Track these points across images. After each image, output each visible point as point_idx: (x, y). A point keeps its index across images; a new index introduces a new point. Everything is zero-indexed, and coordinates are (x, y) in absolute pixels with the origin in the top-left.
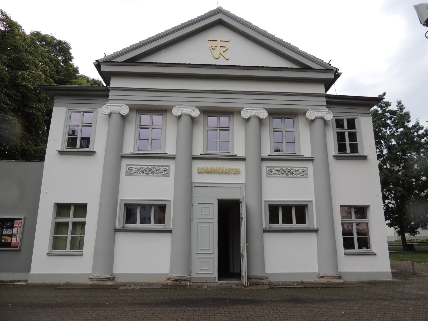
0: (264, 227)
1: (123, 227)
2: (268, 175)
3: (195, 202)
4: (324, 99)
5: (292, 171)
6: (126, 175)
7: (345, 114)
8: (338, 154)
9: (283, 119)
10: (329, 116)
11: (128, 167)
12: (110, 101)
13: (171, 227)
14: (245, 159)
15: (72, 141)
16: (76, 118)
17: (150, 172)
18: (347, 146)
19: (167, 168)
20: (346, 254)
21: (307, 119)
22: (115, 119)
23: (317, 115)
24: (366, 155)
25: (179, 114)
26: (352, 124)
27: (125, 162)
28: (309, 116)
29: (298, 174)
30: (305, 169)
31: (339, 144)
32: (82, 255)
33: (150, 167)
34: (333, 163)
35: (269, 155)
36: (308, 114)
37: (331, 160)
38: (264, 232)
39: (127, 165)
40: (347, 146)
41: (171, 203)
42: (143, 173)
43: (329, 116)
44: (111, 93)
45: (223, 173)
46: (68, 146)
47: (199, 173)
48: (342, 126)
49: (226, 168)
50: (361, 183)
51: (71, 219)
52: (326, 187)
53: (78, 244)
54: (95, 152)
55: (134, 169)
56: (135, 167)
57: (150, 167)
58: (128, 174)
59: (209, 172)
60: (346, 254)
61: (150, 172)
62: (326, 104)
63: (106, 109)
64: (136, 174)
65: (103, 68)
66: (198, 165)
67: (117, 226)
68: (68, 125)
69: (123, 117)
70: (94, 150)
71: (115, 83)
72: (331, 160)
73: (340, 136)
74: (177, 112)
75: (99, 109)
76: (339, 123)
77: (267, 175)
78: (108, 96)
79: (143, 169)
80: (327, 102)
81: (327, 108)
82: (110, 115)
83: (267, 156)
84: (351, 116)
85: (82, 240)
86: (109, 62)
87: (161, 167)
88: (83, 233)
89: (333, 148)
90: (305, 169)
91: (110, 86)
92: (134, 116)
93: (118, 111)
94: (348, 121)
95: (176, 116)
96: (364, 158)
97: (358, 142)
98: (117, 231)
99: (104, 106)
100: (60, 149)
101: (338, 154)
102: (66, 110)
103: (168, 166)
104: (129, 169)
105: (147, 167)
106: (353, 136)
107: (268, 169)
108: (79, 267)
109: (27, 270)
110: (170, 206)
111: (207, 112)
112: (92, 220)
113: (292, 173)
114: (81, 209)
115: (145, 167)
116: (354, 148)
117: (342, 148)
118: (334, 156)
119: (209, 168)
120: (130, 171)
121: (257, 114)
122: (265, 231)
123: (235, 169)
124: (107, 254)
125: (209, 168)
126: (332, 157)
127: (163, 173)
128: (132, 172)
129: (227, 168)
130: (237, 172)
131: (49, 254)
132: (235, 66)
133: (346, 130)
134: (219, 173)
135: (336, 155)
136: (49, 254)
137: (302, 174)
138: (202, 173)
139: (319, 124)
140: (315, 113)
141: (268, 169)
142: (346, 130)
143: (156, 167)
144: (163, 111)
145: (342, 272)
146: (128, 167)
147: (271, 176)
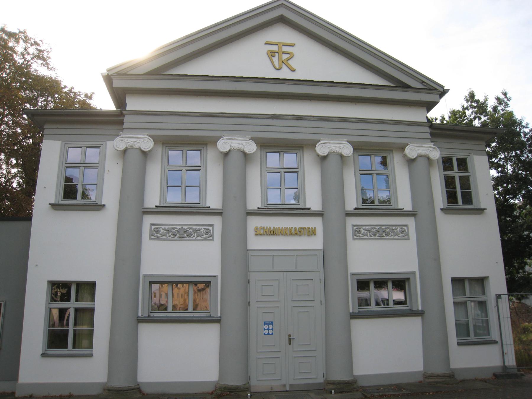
0: (351, 311)
1: (149, 316)
2: (355, 237)
3: (253, 277)
4: (428, 130)
5: (388, 230)
6: (150, 239)
7: (456, 150)
8: (446, 206)
9: (373, 156)
10: (435, 154)
11: (153, 227)
12: (124, 130)
13: (219, 315)
14: (323, 214)
15: (70, 190)
16: (74, 155)
17: (183, 234)
18: (459, 196)
19: (211, 228)
20: (459, 344)
21: (405, 156)
22: (134, 158)
23: (420, 152)
24: (482, 207)
25: (226, 150)
26: (463, 164)
27: (149, 220)
28: (409, 153)
29: (396, 235)
30: (405, 228)
31: (469, 188)
32: (91, 355)
33: (185, 227)
34: (440, 217)
35: (355, 209)
36: (408, 150)
37: (439, 214)
38: (351, 318)
39: (152, 225)
40: (459, 196)
41: (217, 280)
42: (175, 235)
43: (435, 154)
44: (127, 119)
45: (291, 234)
46: (65, 197)
47: (257, 235)
48: (451, 168)
49: (295, 228)
50: (473, 245)
51: (72, 306)
52: (430, 251)
53: (84, 340)
54: (104, 205)
55: (162, 231)
56: (163, 227)
57: (185, 227)
58: (152, 237)
59: (272, 232)
60: (459, 344)
61: (185, 235)
62: (430, 137)
63: (122, 142)
64: (164, 237)
65: (117, 84)
66: (254, 223)
67: (140, 314)
68: (64, 167)
69: (145, 154)
70: (103, 203)
71: (133, 104)
72: (439, 214)
73: (449, 182)
74: (224, 145)
75: (108, 142)
76: (447, 163)
77: (353, 237)
78: (122, 123)
79: (175, 231)
80: (431, 134)
81: (432, 142)
82: (125, 151)
83: (352, 209)
84: (461, 154)
85: (90, 334)
86: (125, 74)
87: (201, 227)
88: (91, 323)
89: (439, 198)
90: (405, 228)
91: (128, 108)
92: (159, 150)
93: (138, 145)
94: (458, 160)
95: (221, 152)
96: (481, 211)
97: (473, 190)
98: (141, 320)
99: (118, 139)
100: (53, 202)
101: (446, 206)
102: (62, 144)
103: (212, 226)
104: (154, 230)
105: (378, 227)
106: (466, 183)
107: (355, 228)
108: (91, 369)
109: (14, 375)
110: (217, 283)
111: (266, 145)
112: (103, 305)
113: (387, 234)
114: (87, 288)
115: (179, 227)
116: (468, 198)
117: (451, 197)
118: (442, 209)
119: (272, 228)
120: (156, 233)
121: (338, 149)
122: (354, 316)
123: (309, 228)
124: (126, 352)
125: (272, 228)
126: (440, 210)
127: (205, 236)
128: (159, 235)
129: (297, 228)
130: (311, 232)
131: (43, 355)
132: (306, 81)
133: (456, 173)
134: (285, 234)
135: (445, 207)
136: (43, 355)
137: (401, 235)
138: (261, 235)
139: (421, 164)
140: (416, 148)
141: (355, 228)
142: (456, 173)
143: (167, 227)
144: (201, 143)
145: (455, 369)
146: (153, 227)
147: (360, 238)
